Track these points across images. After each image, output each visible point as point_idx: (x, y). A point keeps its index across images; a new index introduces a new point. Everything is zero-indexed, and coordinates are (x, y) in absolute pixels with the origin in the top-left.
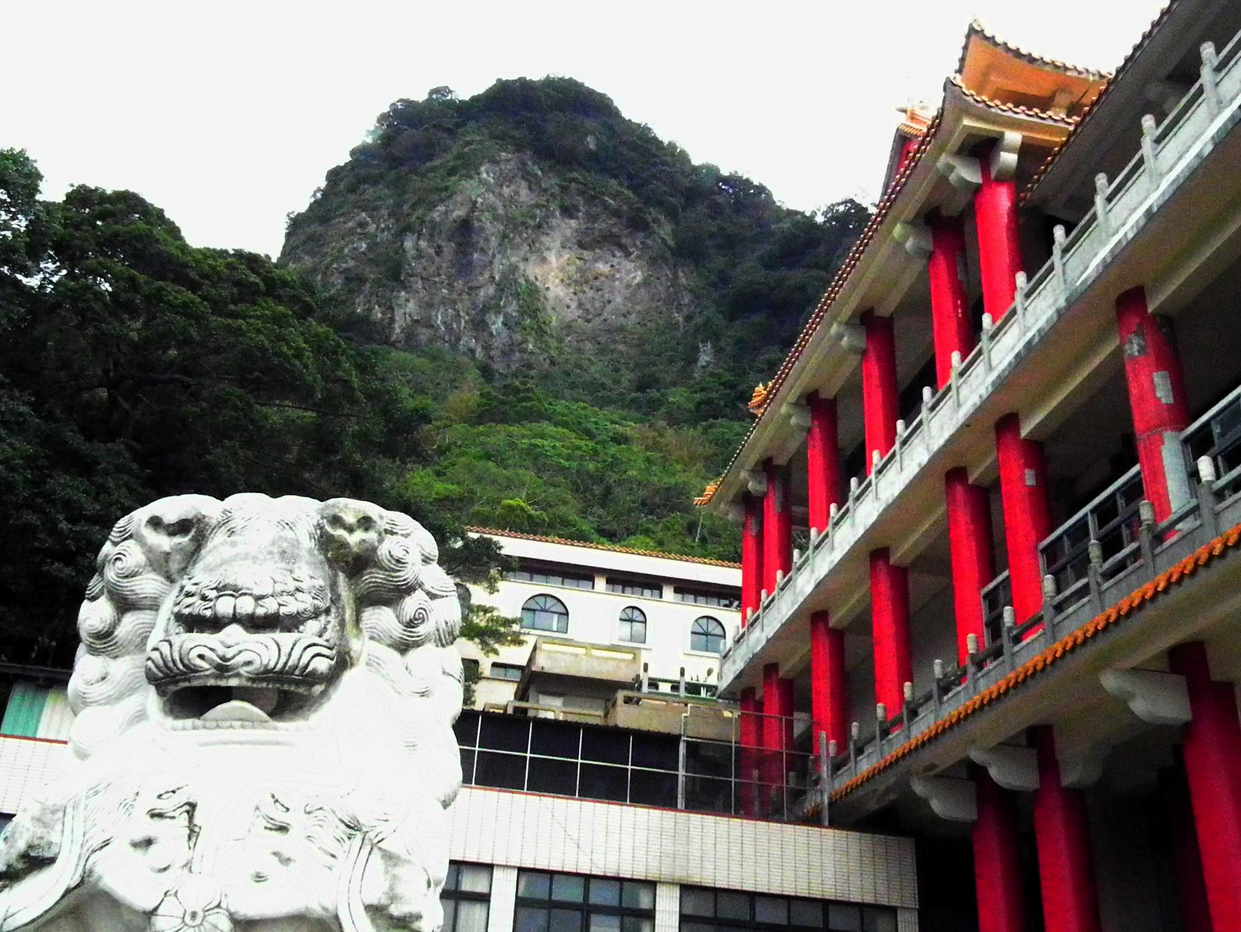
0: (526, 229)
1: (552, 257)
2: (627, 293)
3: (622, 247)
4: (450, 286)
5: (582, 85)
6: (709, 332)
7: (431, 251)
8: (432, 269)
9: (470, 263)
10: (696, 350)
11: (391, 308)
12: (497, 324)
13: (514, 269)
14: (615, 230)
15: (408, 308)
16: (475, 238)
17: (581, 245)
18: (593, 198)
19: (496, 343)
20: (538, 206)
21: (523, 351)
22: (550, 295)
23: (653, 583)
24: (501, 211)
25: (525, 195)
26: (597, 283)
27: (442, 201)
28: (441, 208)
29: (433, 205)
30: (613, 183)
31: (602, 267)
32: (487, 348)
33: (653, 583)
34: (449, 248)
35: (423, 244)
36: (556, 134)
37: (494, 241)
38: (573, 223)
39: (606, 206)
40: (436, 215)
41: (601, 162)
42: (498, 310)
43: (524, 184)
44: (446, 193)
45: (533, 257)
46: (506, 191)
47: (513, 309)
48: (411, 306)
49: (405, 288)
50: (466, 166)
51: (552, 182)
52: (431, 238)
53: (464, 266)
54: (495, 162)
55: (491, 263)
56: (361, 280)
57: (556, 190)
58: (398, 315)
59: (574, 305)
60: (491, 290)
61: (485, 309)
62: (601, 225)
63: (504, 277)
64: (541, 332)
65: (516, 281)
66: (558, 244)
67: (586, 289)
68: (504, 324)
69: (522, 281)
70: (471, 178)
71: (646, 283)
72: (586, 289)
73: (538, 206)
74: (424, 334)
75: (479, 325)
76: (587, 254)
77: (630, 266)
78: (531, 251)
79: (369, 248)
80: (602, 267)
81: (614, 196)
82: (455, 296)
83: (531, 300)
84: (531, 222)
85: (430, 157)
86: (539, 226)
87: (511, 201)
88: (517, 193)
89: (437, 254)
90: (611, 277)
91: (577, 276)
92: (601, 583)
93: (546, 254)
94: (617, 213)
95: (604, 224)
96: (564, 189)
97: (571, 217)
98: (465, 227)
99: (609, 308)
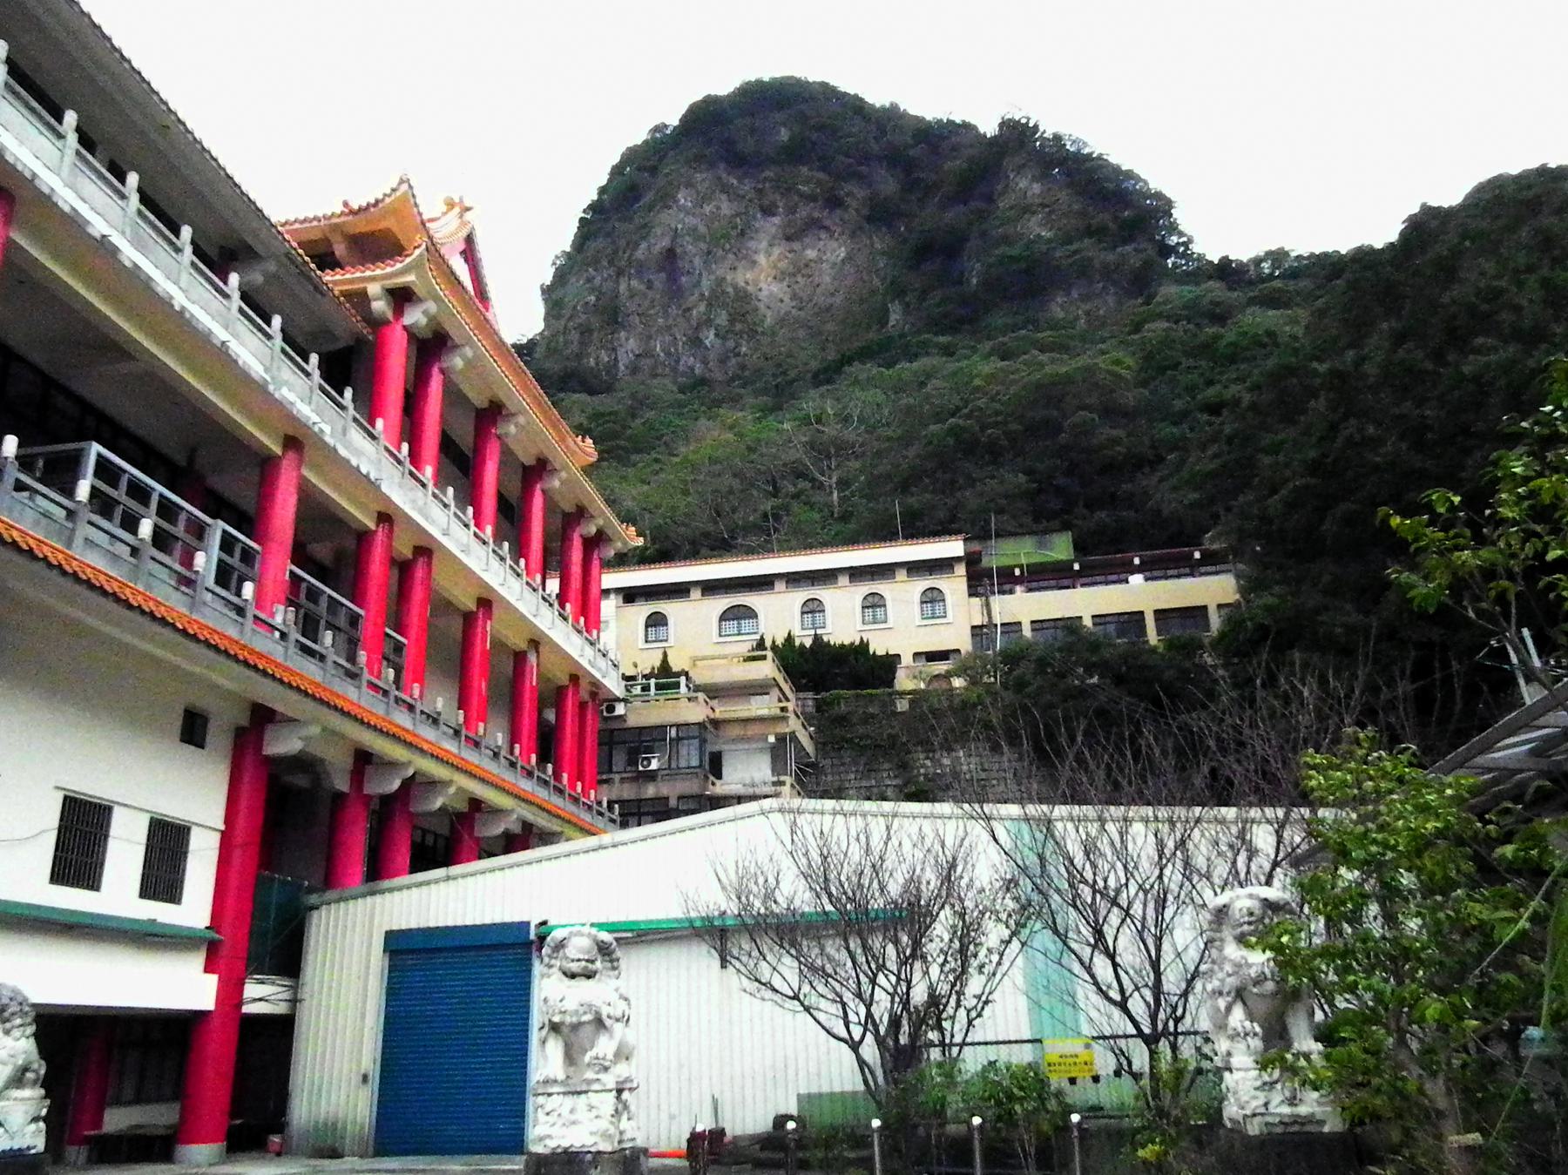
0: (731, 239)
1: (762, 259)
2: (833, 272)
3: (826, 228)
4: (666, 315)
5: (759, 83)
6: (897, 290)
7: (642, 287)
8: (647, 303)
9: (680, 288)
10: (885, 313)
11: (614, 349)
12: (709, 338)
13: (721, 281)
14: (816, 215)
15: (629, 345)
16: (680, 264)
17: (788, 239)
18: (789, 190)
19: (712, 356)
20: (737, 215)
21: (738, 355)
22: (763, 295)
23: (826, 577)
24: (702, 229)
25: (726, 208)
26: (808, 271)
27: (643, 238)
28: (644, 245)
29: (637, 245)
30: (804, 170)
31: (811, 254)
32: (705, 362)
33: (826, 577)
34: (659, 280)
35: (634, 283)
36: (773, 142)
37: (697, 261)
38: (776, 220)
39: (801, 195)
40: (640, 254)
41: (795, 154)
42: (708, 322)
43: (724, 197)
44: (645, 230)
45: (741, 265)
46: (707, 209)
47: (722, 318)
48: (632, 344)
49: (624, 327)
50: (666, 199)
51: (747, 187)
52: (640, 273)
53: (675, 292)
54: (689, 185)
55: (699, 282)
56: (590, 331)
57: (752, 195)
58: (621, 353)
59: (787, 299)
60: (702, 308)
61: (697, 328)
62: (803, 212)
63: (713, 291)
64: (752, 333)
65: (723, 292)
66: (764, 244)
67: (799, 279)
68: (717, 335)
69: (730, 290)
70: (670, 208)
71: (849, 258)
72: (799, 279)
73: (737, 215)
74: (646, 363)
75: (696, 342)
76: (796, 246)
77: (835, 244)
78: (739, 260)
79: (598, 299)
80: (811, 254)
81: (807, 182)
82: (670, 321)
83: (741, 305)
84: (734, 233)
85: (637, 199)
86: (742, 233)
87: (715, 216)
88: (718, 208)
89: (649, 288)
90: (820, 260)
91: (791, 269)
92: (696, 593)
93: (756, 257)
94: (812, 198)
95: (803, 212)
96: (760, 191)
97: (774, 215)
98: (670, 254)
99: (819, 290)
